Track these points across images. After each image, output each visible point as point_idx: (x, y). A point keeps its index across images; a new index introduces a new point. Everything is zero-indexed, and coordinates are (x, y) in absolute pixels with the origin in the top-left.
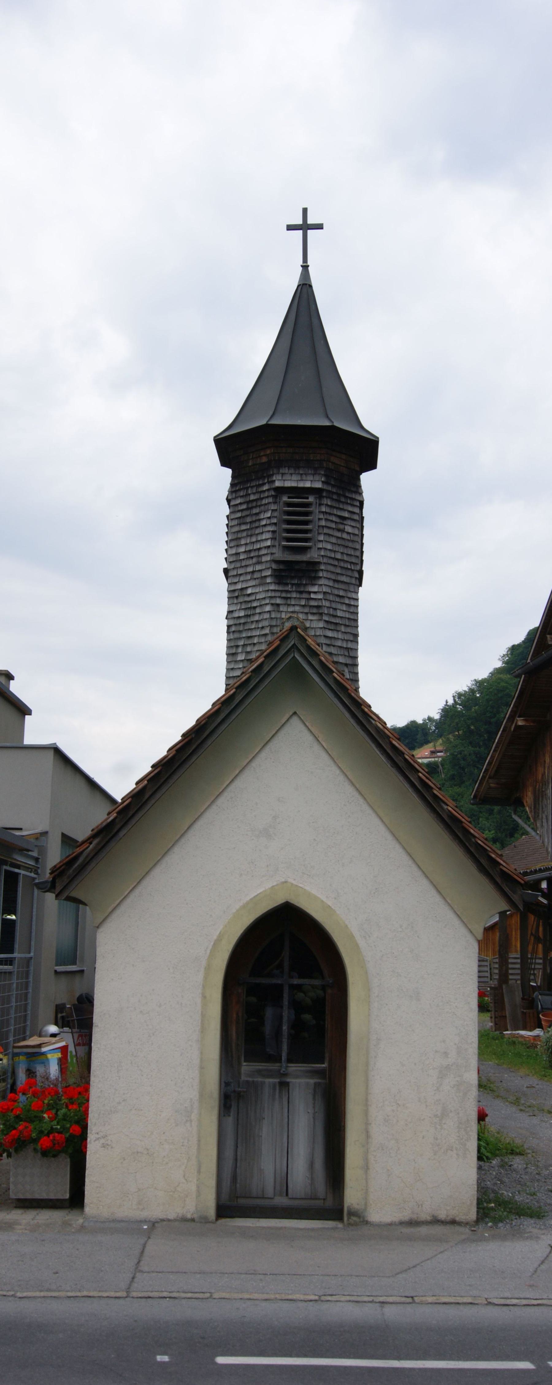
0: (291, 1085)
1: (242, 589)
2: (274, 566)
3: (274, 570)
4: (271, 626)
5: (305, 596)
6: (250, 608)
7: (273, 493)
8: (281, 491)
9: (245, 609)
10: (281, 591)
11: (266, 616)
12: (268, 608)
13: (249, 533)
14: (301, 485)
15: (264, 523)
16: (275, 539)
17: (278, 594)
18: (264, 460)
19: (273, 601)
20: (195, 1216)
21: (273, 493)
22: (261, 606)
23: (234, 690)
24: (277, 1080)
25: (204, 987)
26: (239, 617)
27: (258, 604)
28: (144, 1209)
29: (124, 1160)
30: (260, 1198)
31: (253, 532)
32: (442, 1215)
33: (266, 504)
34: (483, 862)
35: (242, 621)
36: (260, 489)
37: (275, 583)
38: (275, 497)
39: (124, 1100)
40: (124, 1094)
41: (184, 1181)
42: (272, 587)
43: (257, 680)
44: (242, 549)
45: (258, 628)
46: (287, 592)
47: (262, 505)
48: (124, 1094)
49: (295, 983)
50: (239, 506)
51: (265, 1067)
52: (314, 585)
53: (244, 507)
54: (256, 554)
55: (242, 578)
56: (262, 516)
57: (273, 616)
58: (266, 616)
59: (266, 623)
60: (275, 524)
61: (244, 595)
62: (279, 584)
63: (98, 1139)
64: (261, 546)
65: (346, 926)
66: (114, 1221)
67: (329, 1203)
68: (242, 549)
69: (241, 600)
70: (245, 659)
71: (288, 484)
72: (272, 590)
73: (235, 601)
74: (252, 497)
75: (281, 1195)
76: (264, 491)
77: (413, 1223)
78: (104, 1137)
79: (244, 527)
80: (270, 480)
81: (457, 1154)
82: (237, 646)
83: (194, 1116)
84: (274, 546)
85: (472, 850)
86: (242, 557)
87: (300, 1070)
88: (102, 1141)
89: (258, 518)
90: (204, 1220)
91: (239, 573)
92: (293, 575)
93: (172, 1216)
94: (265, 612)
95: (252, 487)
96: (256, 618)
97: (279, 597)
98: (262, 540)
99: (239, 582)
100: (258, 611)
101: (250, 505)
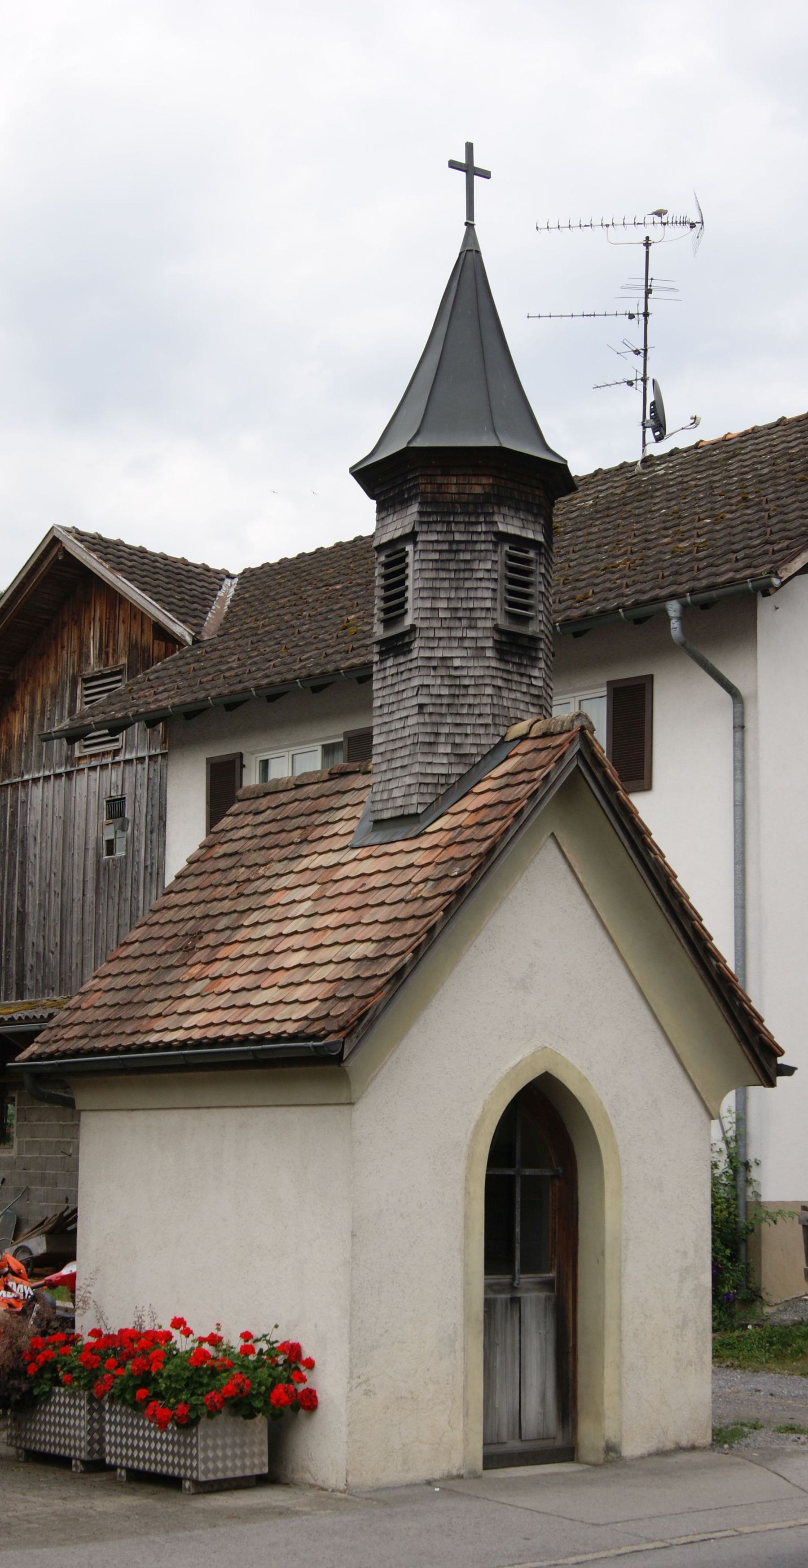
0: (522, 1301)
1: (443, 659)
2: (496, 637)
3: (495, 641)
4: (494, 715)
5: (525, 680)
6: (459, 686)
7: (494, 539)
8: (502, 537)
9: (450, 686)
10: (504, 670)
11: (486, 700)
12: (489, 691)
13: (454, 584)
14: (524, 535)
15: (480, 575)
16: (496, 599)
17: (500, 674)
18: (478, 490)
19: (495, 682)
20: (462, 1472)
21: (494, 539)
22: (476, 685)
23: (526, 801)
24: (508, 1296)
25: (467, 1180)
26: (440, 696)
27: (473, 683)
28: (409, 1469)
29: (388, 1408)
30: (495, 1444)
31: (461, 584)
32: (684, 1443)
33: (481, 551)
34: (745, 1028)
35: (445, 701)
36: (471, 529)
37: (496, 658)
38: (495, 544)
39: (386, 1331)
40: (386, 1323)
41: (449, 1428)
42: (494, 664)
43: (545, 791)
44: (443, 604)
45: (473, 714)
46: (508, 672)
47: (475, 551)
48: (386, 1323)
49: (527, 1173)
50: (435, 544)
51: (496, 1281)
52: (534, 667)
53: (445, 547)
54: (468, 614)
55: (442, 644)
56: (475, 566)
57: (495, 702)
58: (486, 700)
59: (487, 710)
60: (496, 580)
61: (448, 667)
62: (500, 660)
63: (360, 1384)
64: (475, 606)
65: (601, 1103)
66: (378, 1489)
67: (559, 1442)
68: (443, 604)
69: (443, 672)
70: (451, 753)
71: (512, 530)
72: (493, 668)
73: (432, 673)
74: (458, 537)
75: (513, 1438)
76: (479, 533)
77: (661, 1453)
78: (366, 1382)
79: (443, 575)
80: (487, 519)
81: (696, 1370)
82: (437, 734)
83: (458, 1345)
84: (494, 609)
85: (736, 1014)
86: (442, 614)
87: (530, 1282)
88: (364, 1387)
89: (468, 566)
90: (475, 1476)
91: (437, 635)
92: (514, 651)
93: (437, 1475)
94: (483, 695)
95: (457, 523)
96: (470, 700)
97: (502, 678)
98: (477, 598)
99: (438, 647)
100: (471, 691)
101: (454, 547)
